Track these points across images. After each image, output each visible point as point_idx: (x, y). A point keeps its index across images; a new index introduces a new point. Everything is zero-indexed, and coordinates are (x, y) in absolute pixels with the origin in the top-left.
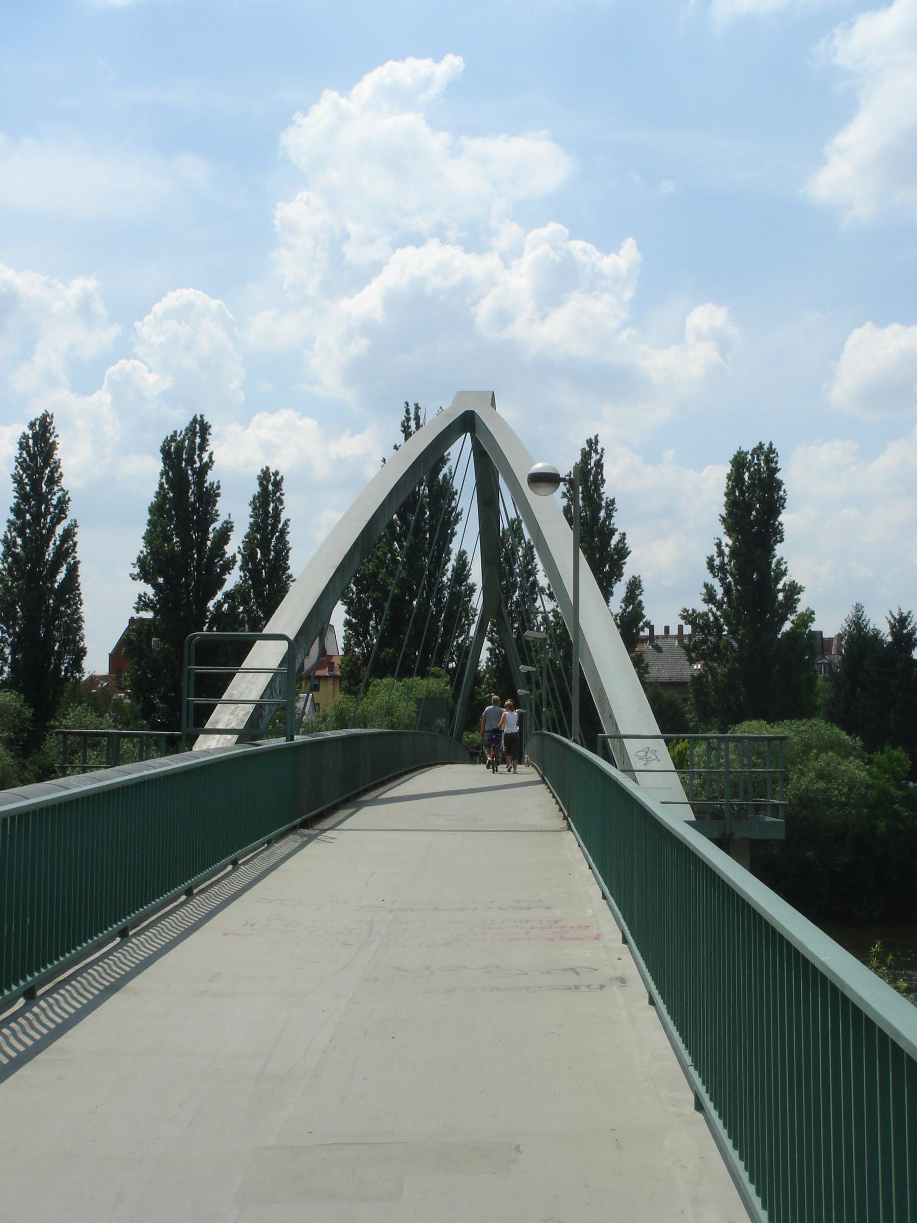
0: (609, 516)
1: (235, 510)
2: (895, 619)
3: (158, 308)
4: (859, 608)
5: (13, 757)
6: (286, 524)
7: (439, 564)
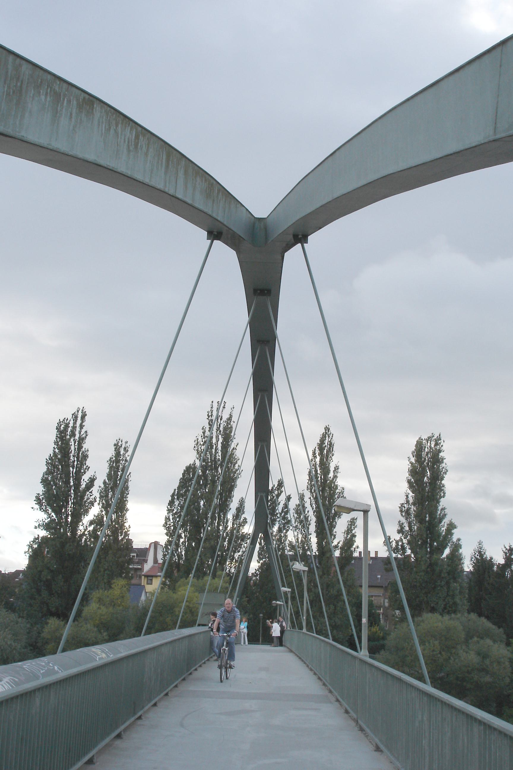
0: (335, 477)
1: (97, 468)
2: (506, 549)
3: (105, 516)
4: (480, 543)
5: (62, 621)
6: (130, 473)
7: (224, 507)
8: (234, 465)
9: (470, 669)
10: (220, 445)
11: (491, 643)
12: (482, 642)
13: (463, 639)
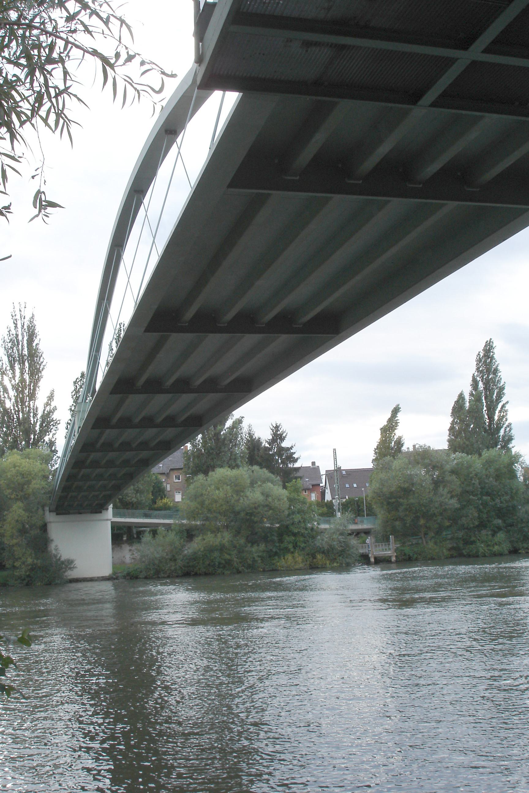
8: (40, 358)
9: (256, 505)
10: (25, 342)
11: (272, 486)
12: (264, 485)
13: (249, 485)
